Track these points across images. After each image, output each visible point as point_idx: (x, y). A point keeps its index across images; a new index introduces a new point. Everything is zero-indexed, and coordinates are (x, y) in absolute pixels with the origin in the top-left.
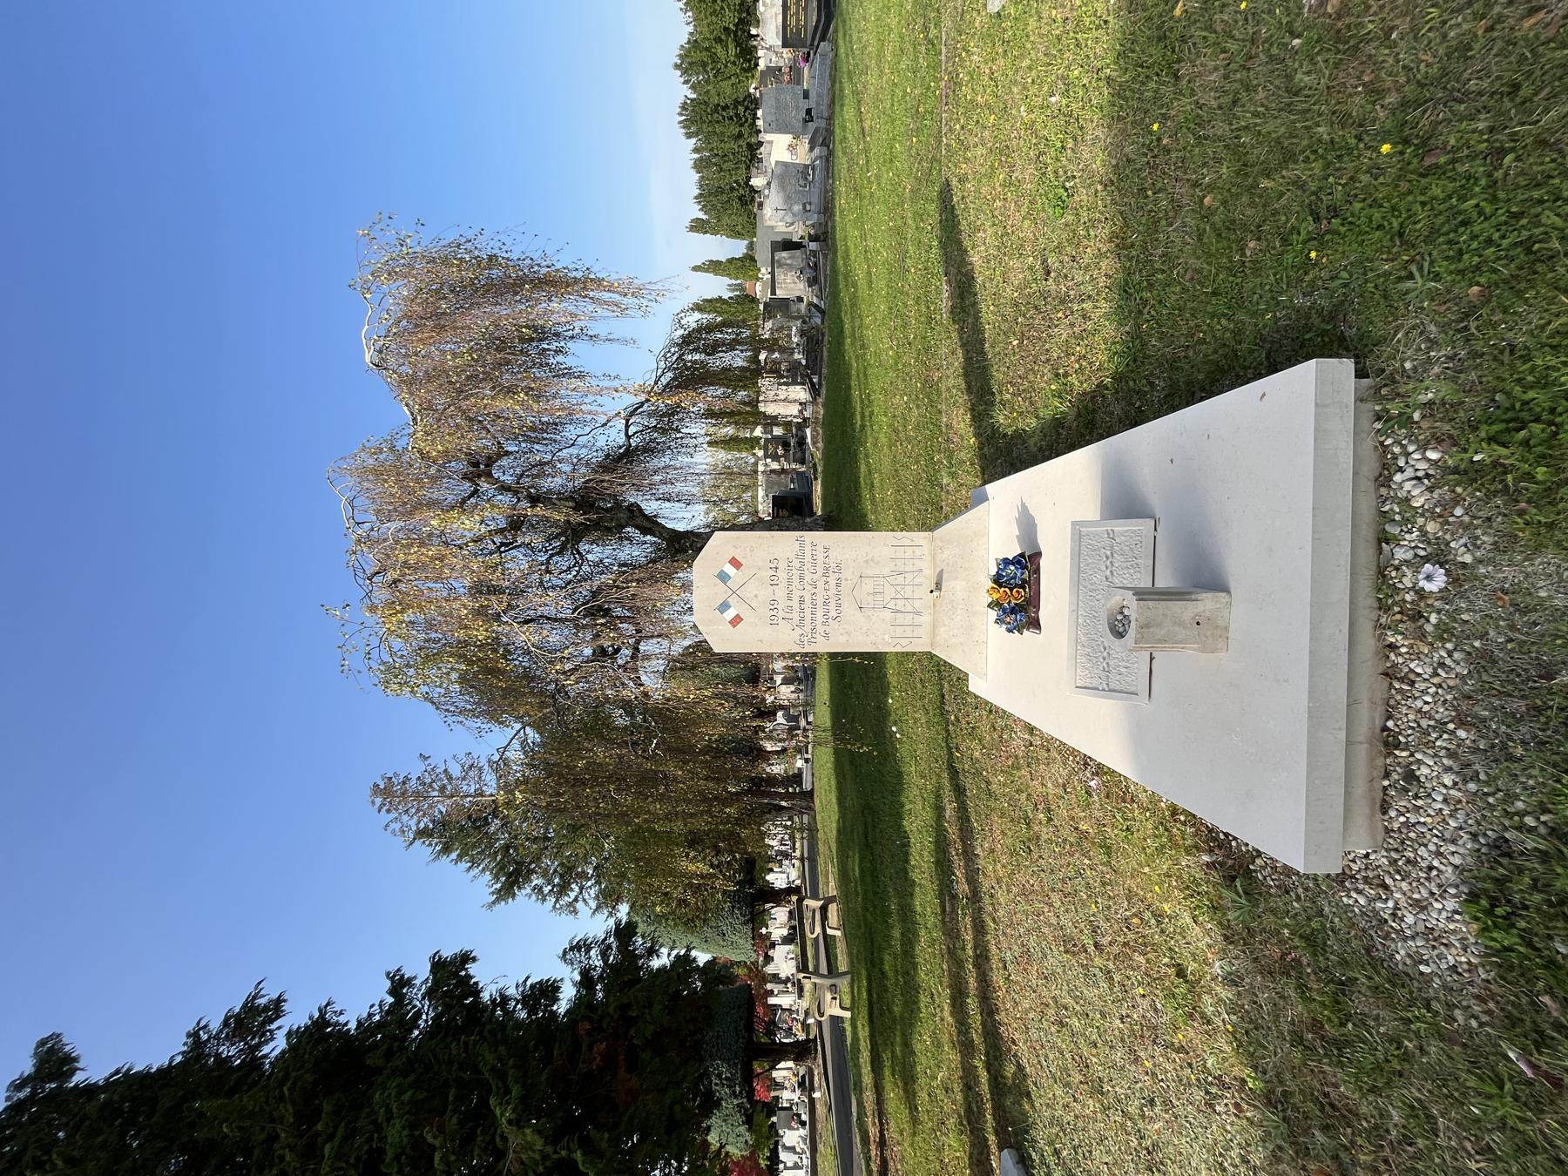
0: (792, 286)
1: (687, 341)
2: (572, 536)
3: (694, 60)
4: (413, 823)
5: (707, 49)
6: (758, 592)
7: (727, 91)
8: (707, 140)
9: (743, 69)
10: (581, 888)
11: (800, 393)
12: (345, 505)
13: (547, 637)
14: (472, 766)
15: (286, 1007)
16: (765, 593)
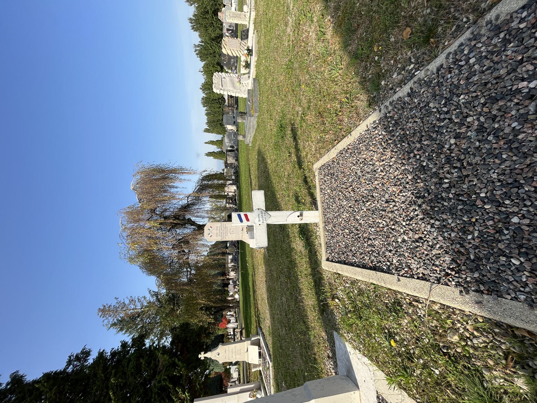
2: (174, 226)
4: (112, 320)
6: (215, 232)
10: (167, 339)
12: (120, 223)
13: (168, 251)
14: (132, 300)
15: (91, 353)
16: (216, 232)
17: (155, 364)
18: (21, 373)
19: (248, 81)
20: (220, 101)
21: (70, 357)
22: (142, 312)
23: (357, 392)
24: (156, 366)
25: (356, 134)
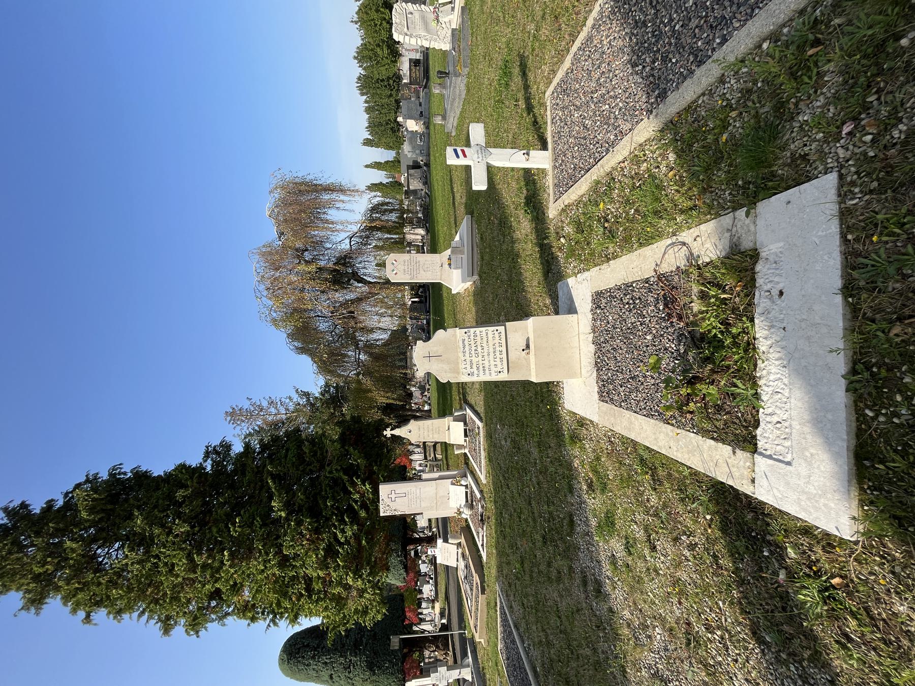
0: (416, 185)
1: (374, 209)
3: (364, 55)
5: (372, 50)
6: (401, 267)
7: (384, 72)
8: (373, 96)
9: (392, 61)
11: (421, 231)
12: (252, 270)
17: (322, 454)
18: (144, 469)
19: (451, 17)
20: (391, 82)
21: (207, 447)
22: (287, 419)
23: (575, 315)
24: (324, 458)
25: (590, 22)
